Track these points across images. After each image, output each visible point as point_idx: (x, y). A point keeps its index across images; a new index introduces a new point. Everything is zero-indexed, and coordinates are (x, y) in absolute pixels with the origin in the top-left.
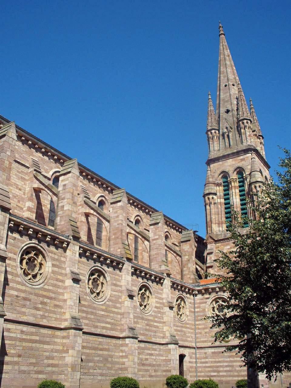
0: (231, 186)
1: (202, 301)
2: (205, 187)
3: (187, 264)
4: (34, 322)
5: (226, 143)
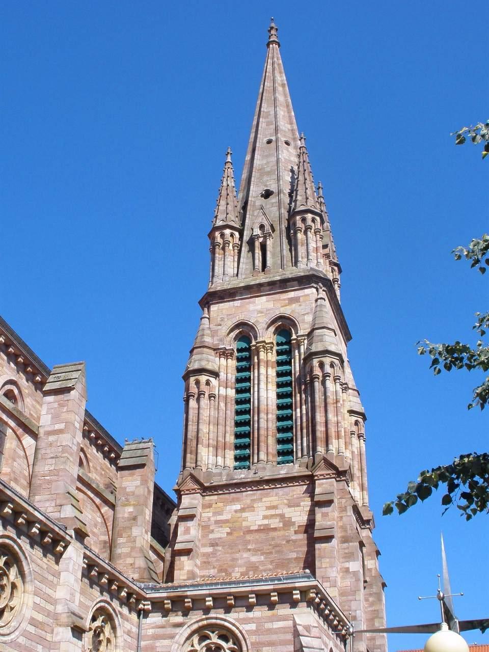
0: (256, 360)
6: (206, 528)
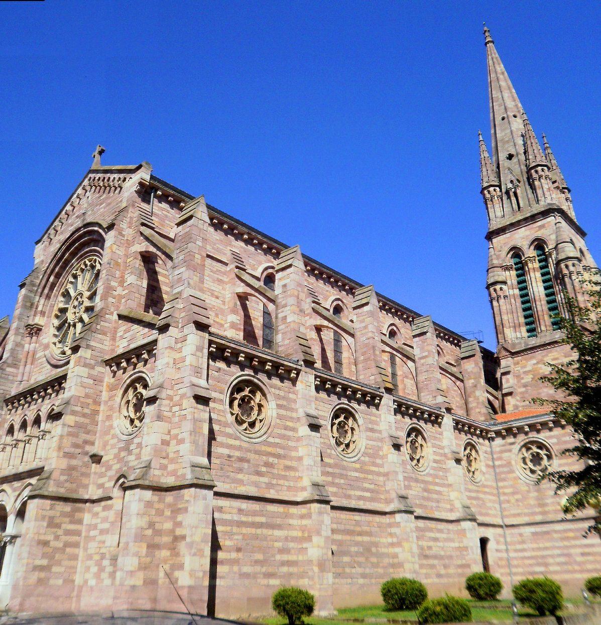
1: (503, 448)
2: (488, 274)
3: (474, 392)
4: (256, 495)
5: (514, 205)
6: (518, 377)
